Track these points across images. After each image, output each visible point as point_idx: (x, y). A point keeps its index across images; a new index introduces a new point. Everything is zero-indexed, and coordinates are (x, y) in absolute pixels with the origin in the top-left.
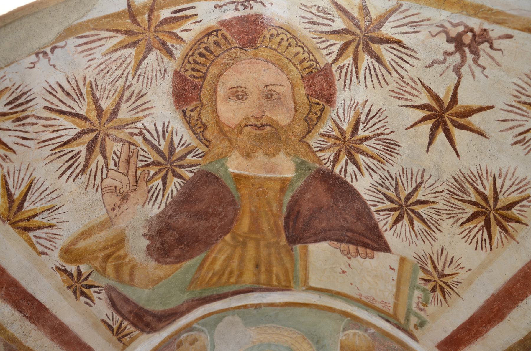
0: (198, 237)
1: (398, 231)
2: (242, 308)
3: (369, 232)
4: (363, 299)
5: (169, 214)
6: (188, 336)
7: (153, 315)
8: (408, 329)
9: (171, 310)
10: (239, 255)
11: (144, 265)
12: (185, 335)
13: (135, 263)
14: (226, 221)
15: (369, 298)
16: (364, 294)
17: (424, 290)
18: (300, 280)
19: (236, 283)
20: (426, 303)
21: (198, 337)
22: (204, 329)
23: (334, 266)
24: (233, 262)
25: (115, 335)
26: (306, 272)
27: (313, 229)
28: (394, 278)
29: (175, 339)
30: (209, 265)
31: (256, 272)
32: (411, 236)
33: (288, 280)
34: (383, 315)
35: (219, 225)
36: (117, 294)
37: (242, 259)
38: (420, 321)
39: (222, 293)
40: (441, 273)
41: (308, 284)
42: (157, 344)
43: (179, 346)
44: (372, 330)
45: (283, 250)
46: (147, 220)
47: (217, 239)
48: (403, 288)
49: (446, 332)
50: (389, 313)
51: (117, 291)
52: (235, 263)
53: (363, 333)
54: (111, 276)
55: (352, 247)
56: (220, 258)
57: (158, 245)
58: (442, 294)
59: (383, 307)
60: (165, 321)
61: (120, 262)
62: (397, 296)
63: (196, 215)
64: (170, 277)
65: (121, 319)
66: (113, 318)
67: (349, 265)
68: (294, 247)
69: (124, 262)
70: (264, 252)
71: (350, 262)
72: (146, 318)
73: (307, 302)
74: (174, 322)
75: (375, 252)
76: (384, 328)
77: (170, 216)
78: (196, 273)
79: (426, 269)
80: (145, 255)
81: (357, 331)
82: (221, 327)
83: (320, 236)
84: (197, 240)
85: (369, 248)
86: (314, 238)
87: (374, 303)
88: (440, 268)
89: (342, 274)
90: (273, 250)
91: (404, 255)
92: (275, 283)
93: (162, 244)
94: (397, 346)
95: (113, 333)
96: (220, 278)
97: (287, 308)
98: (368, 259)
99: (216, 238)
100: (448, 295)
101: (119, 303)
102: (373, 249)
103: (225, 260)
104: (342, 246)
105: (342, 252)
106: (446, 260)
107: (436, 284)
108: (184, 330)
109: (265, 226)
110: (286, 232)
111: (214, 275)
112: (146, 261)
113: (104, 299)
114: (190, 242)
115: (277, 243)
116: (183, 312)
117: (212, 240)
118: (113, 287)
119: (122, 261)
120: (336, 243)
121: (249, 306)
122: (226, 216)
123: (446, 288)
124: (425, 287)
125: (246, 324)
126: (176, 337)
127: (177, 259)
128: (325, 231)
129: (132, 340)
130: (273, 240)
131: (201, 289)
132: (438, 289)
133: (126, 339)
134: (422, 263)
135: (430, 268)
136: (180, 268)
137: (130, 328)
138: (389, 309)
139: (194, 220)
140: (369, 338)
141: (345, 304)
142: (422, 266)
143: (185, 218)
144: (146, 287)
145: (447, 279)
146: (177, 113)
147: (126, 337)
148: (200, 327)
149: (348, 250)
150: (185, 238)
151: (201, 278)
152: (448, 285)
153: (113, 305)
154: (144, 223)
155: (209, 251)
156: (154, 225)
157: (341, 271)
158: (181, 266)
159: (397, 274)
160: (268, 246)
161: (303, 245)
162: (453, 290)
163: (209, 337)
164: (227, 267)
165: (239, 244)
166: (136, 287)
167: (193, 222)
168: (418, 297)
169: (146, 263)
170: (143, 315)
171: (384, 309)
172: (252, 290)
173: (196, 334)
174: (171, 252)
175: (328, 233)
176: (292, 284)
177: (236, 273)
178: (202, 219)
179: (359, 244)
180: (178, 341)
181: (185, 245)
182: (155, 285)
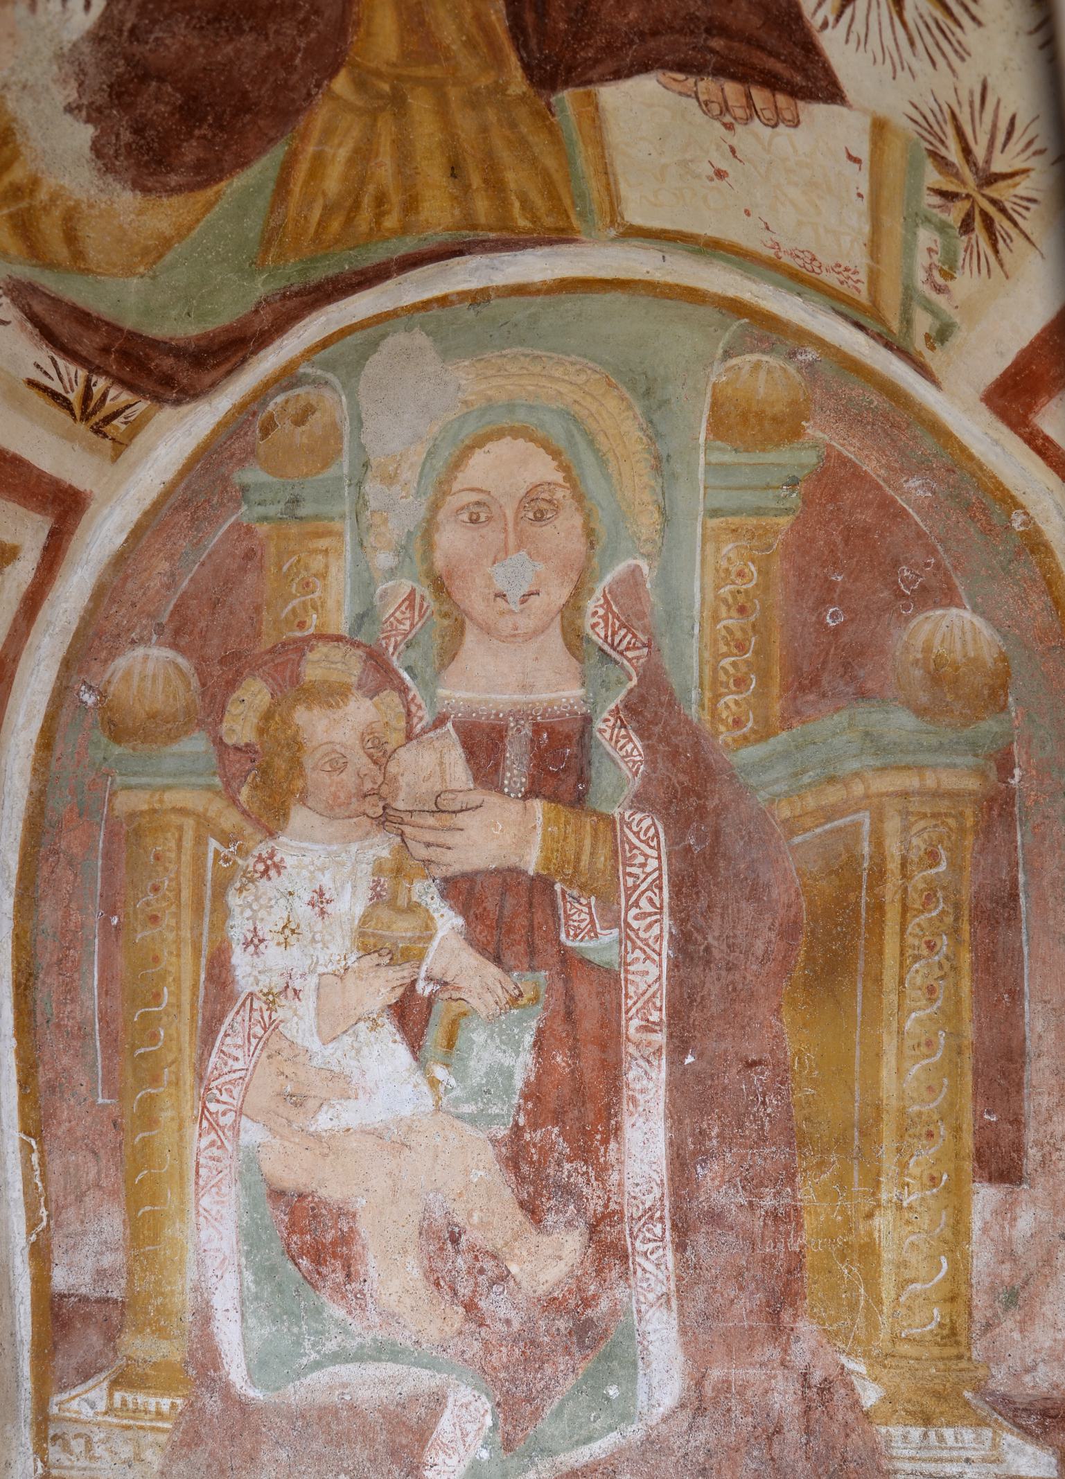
0: (244, 94)
1: (859, 27)
2: (435, 305)
3: (776, 34)
4: (786, 259)
5: (129, 25)
6: (287, 401)
7: (177, 351)
8: (911, 350)
9: (227, 330)
10: (394, 141)
11: (103, 206)
12: (280, 399)
13: (72, 203)
14: (321, 27)
15: (801, 255)
16: (786, 245)
17: (942, 228)
18: (595, 207)
19: (404, 230)
20: (950, 268)
21: (314, 403)
22: (330, 376)
23: (688, 156)
24: (380, 165)
25: (81, 419)
26: (608, 179)
27: (602, 31)
28: (862, 193)
29: (254, 414)
30: (306, 183)
31: (456, 192)
32: (897, 45)
33: (557, 207)
34: (843, 308)
35: (303, 45)
36: (49, 302)
37: (404, 154)
38: (937, 324)
39: (367, 264)
40: (984, 170)
41: (623, 218)
42: (208, 432)
43: (267, 429)
44: (811, 355)
45: (522, 113)
46: (63, 55)
47: (309, 95)
48: (887, 221)
49: (1002, 354)
50: (858, 302)
51: (45, 294)
52: (384, 169)
53: (781, 363)
54: (13, 251)
55: (732, 90)
56: (334, 155)
57: (126, 136)
58: (990, 238)
59: (842, 283)
60: (214, 367)
61: (24, 204)
62: (874, 247)
63: (217, 19)
64: (194, 233)
65: (82, 373)
66: (59, 374)
67: (733, 151)
68: (553, 100)
69: (36, 203)
70: (466, 123)
71: (734, 142)
72: (157, 361)
73: (623, 276)
74: (246, 365)
75: (801, 104)
76: (846, 348)
77: (132, 31)
78: (272, 212)
79: (943, 158)
80: (95, 173)
81: (765, 358)
82: (374, 366)
83: (629, 56)
84: (245, 105)
85: (783, 91)
86: (611, 65)
87: (817, 270)
88: (979, 152)
89: (717, 181)
90: (491, 115)
91: (882, 112)
92: (522, 223)
93: (138, 131)
94: (876, 400)
95: (73, 414)
96: (349, 221)
97: (563, 296)
98: (782, 128)
99: (304, 91)
100: (1005, 241)
101: (65, 329)
102: (796, 93)
103: (351, 162)
104: (702, 85)
105: (705, 105)
106: (995, 126)
107: (972, 207)
108: (277, 385)
109: (449, 34)
110: (518, 49)
111: (328, 211)
112: (101, 191)
113: (14, 322)
114: (224, 112)
115: (499, 89)
116: (262, 333)
117: (293, 100)
118: (30, 283)
119: (27, 200)
120: (681, 77)
121: (454, 298)
122: (317, 12)
123: (1000, 221)
124: (944, 216)
125: (447, 353)
126: (254, 407)
127: (198, 174)
128: (641, 34)
129: (135, 428)
130: (484, 81)
131: (301, 261)
132: (978, 223)
133: (117, 428)
134: (931, 138)
135: (953, 153)
136: (217, 200)
137: (118, 397)
138: (857, 289)
139: (217, 35)
140: (798, 378)
141: (738, 278)
142: (930, 147)
143: (183, 31)
144: (129, 271)
145: (999, 191)
147: (115, 422)
148: (319, 372)
149: (721, 100)
150: (205, 100)
151: (290, 227)
152: (1003, 210)
153: (48, 335)
154: (55, 68)
155: (294, 138)
156: (91, 70)
157: (711, 172)
158: (218, 195)
159: (867, 177)
160: (474, 102)
161: (581, 90)
162: (1015, 224)
163: (343, 398)
164: (363, 181)
165: (381, 103)
166: (99, 274)
167: (217, 44)
168: (930, 250)
169: (104, 197)
170: (146, 355)
171: (843, 289)
172: (457, 248)
173: (308, 393)
174: (173, 152)
175: (652, 44)
176: (576, 222)
177: (396, 199)
178: (240, 31)
179: (753, 77)
180: (262, 416)
181: (210, 125)
182: (155, 263)
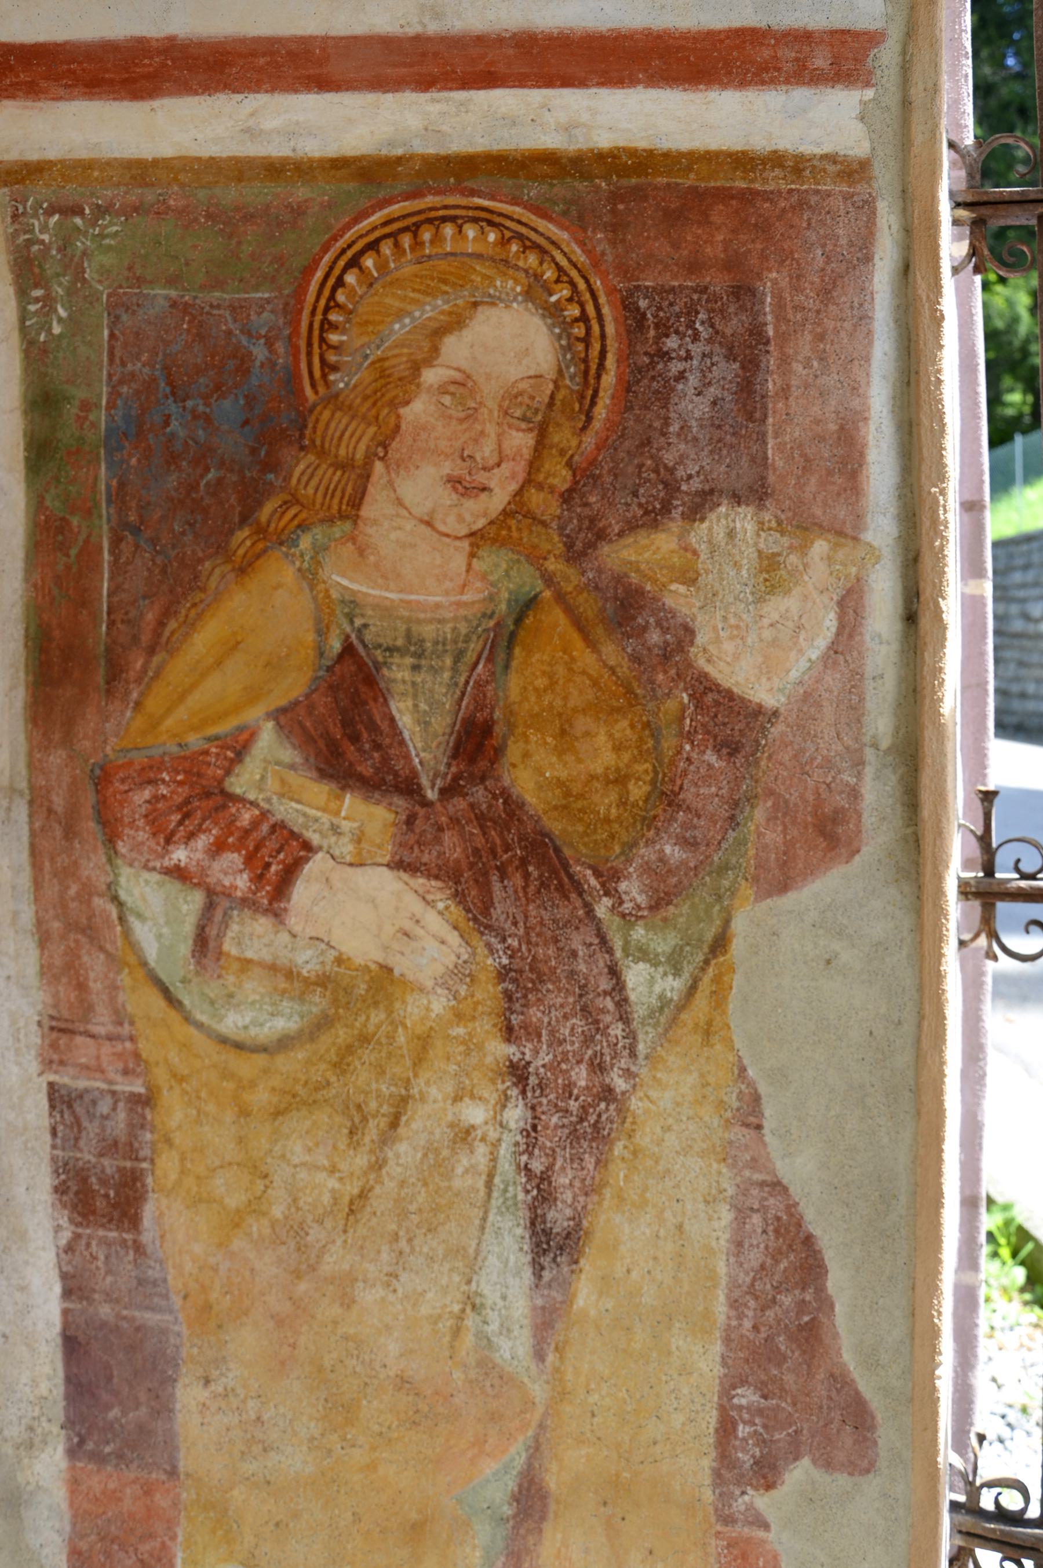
146: (900, 772)
